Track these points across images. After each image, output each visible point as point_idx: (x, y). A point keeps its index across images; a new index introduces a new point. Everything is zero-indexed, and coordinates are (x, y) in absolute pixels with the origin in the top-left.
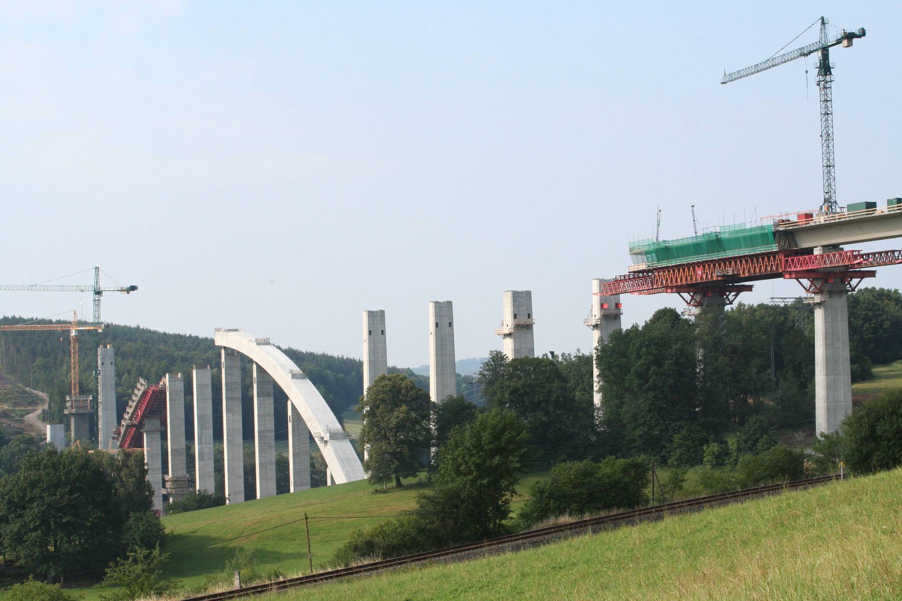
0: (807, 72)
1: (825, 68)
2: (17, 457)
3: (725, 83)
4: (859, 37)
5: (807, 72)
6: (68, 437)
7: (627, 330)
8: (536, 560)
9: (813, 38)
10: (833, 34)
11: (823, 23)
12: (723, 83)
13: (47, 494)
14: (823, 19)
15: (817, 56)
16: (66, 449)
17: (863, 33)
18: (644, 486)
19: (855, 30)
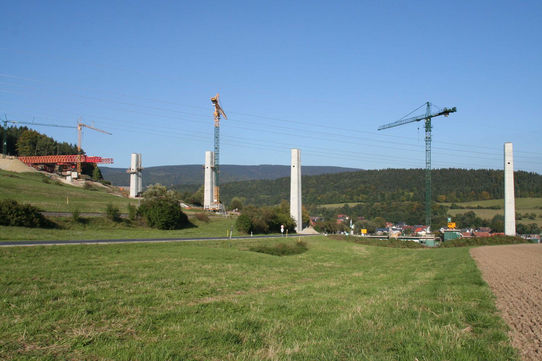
0: (418, 129)
1: (428, 127)
2: (469, 188)
3: (380, 130)
4: (452, 112)
5: (418, 129)
6: (68, 171)
7: (478, 218)
8: (267, 231)
9: (422, 112)
10: (434, 111)
11: (428, 106)
12: (378, 130)
13: (153, 332)
14: (428, 103)
15: (423, 122)
16: (258, 194)
17: (454, 110)
18: (4, 129)
19: (450, 107)
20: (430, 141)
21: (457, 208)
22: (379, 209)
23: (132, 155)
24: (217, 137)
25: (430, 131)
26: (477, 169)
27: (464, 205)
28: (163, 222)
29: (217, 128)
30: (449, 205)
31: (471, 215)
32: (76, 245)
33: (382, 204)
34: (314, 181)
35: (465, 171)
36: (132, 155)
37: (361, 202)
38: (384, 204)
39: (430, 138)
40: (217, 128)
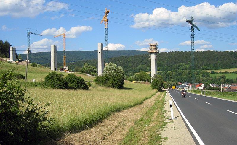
20: (193, 37)
21: (214, 73)
22: (171, 75)
23: (51, 46)
24: (106, 34)
25: (193, 32)
26: (224, 51)
27: (218, 71)
28: (119, 85)
29: (106, 29)
30: (210, 71)
31: (224, 77)
32: (210, 95)
33: (173, 72)
34: (131, 59)
35: (217, 52)
36: (51, 46)
37: (159, 71)
38: (173, 72)
39: (193, 36)
40: (106, 29)
